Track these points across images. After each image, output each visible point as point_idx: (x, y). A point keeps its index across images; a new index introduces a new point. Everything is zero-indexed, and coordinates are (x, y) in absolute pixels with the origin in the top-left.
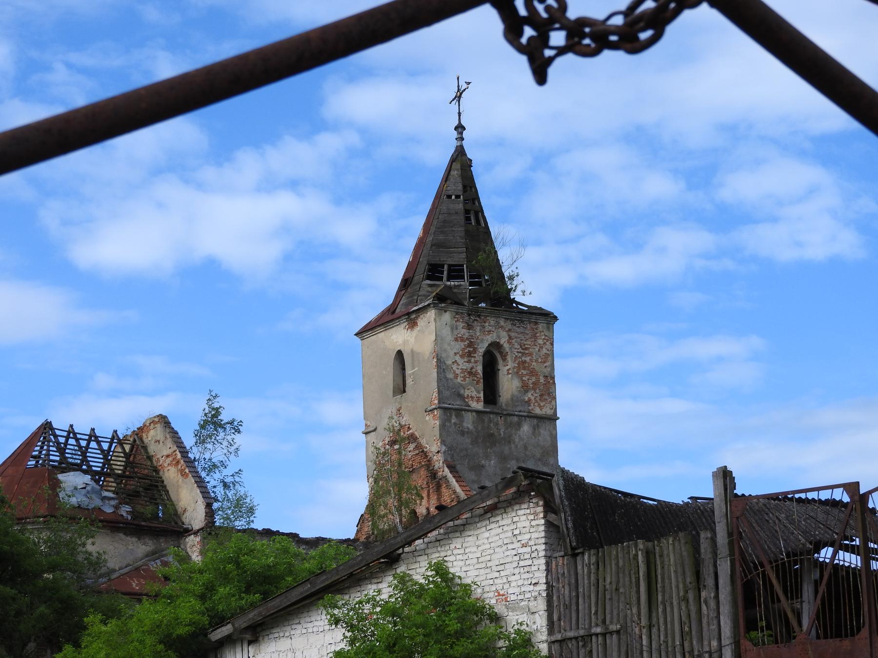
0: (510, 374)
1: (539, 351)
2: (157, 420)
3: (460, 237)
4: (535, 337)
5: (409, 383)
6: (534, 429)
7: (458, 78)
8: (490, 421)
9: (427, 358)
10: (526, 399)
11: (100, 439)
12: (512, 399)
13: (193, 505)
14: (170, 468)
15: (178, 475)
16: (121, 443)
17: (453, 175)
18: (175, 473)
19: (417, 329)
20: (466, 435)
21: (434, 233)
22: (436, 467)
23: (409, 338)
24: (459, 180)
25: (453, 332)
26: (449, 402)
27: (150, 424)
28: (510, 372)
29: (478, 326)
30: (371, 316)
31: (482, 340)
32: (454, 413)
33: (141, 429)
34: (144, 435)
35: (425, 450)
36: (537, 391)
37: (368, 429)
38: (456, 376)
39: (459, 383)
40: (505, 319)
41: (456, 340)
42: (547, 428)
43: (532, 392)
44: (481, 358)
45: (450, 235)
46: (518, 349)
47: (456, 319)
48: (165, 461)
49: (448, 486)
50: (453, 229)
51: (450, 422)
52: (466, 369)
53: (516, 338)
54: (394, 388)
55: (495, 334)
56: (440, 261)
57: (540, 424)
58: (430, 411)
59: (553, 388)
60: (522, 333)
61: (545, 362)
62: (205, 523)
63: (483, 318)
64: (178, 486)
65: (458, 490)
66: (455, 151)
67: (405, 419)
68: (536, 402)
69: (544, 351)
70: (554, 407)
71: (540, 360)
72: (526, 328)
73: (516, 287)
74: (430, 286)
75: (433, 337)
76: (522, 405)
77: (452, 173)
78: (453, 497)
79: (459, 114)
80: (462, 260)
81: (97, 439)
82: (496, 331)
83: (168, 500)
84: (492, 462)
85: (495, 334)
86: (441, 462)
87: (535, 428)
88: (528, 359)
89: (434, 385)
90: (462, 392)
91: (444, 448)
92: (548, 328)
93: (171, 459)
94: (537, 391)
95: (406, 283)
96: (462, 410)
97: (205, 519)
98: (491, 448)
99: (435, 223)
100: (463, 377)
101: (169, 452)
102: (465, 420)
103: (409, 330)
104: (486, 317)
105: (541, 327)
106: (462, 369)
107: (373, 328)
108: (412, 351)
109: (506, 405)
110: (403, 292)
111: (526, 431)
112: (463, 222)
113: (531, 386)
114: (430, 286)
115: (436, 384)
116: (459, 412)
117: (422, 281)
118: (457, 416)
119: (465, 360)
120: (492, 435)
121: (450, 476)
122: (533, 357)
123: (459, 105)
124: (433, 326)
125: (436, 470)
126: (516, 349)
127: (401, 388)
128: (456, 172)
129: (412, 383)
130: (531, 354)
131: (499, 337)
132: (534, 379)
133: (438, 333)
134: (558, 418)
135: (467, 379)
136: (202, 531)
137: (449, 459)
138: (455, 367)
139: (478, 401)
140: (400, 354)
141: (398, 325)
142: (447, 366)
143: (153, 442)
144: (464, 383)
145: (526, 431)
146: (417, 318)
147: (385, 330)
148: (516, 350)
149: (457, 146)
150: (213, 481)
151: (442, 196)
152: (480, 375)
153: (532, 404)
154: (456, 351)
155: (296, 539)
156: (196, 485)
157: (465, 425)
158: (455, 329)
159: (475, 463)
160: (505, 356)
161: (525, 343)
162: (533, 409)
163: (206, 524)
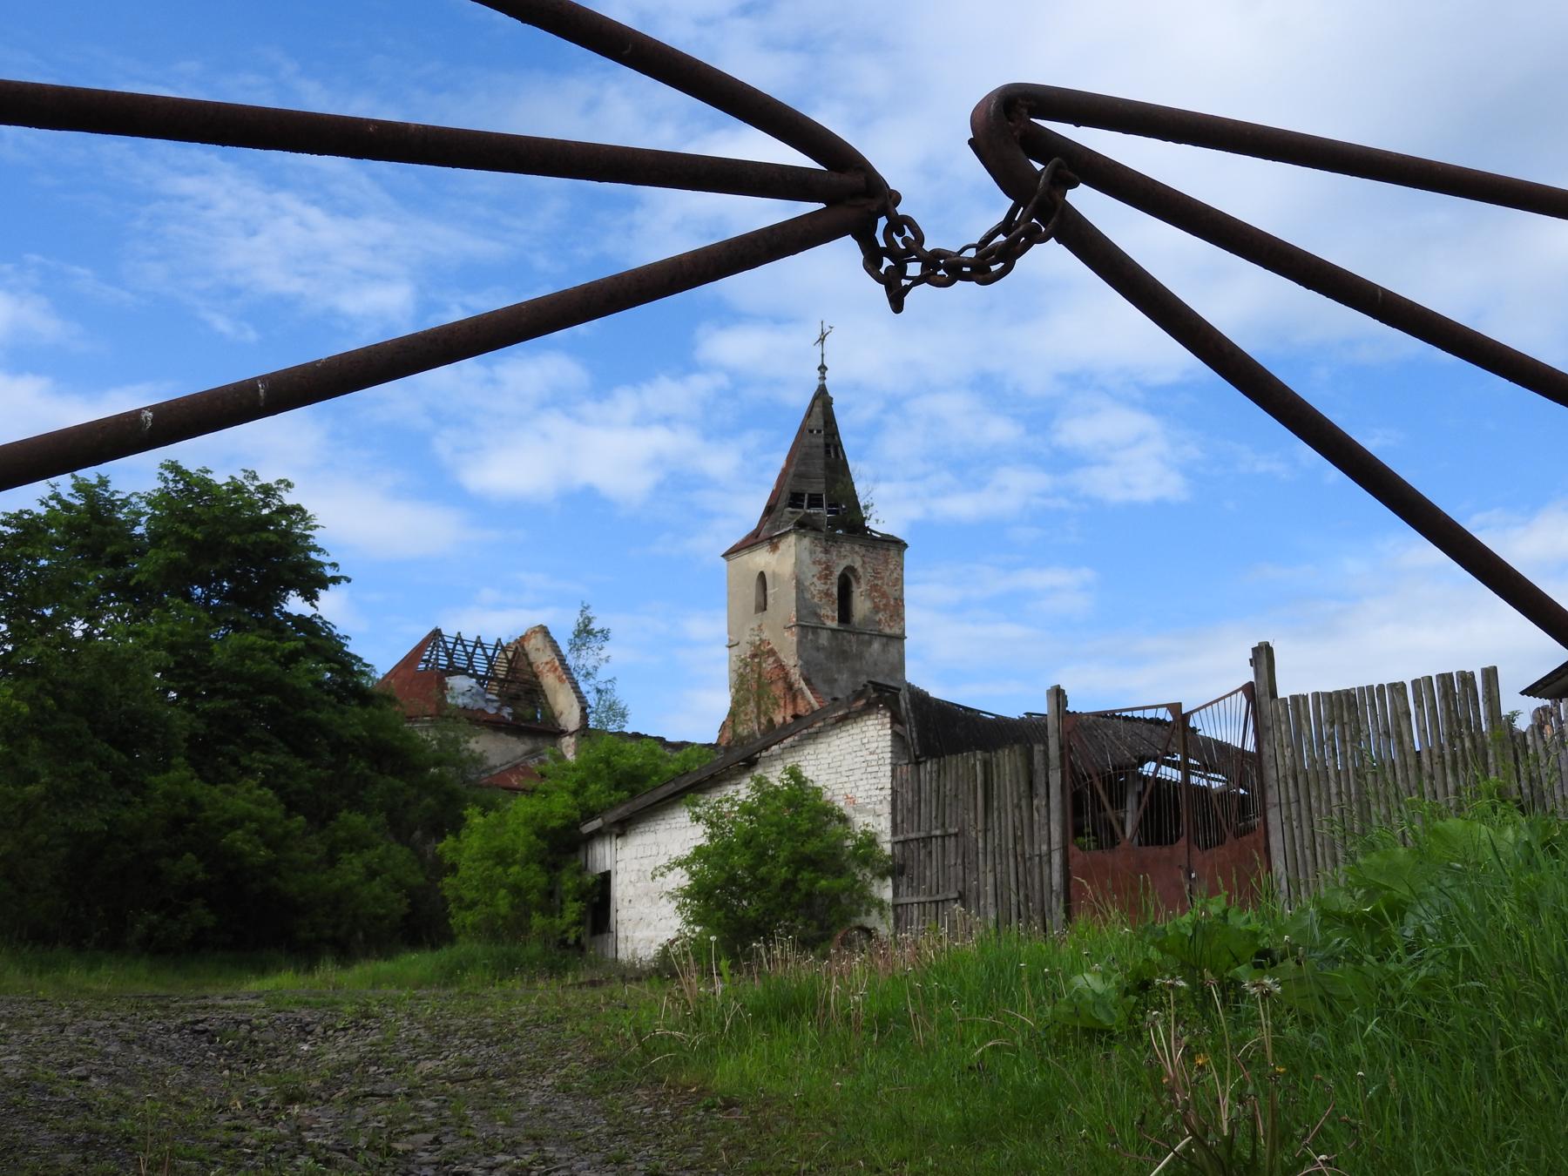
4: (886, 562)
16: (504, 650)
22: (793, 680)
24: (821, 416)
31: (838, 564)
34: (526, 644)
41: (814, 563)
49: (804, 697)
69: (895, 575)
75: (793, 560)
87: (885, 646)
88: (879, 582)
89: (794, 604)
90: (818, 611)
91: (800, 662)
92: (899, 554)
95: (769, 510)
96: (817, 628)
99: (797, 455)
101: (548, 659)
105: (892, 553)
114: (792, 513)
116: (815, 629)
118: (813, 633)
120: (844, 652)
124: (793, 550)
127: (762, 606)
131: (853, 561)
132: (884, 601)
138: (812, 588)
139: (833, 619)
140: (762, 575)
146: (779, 542)
157: (821, 641)
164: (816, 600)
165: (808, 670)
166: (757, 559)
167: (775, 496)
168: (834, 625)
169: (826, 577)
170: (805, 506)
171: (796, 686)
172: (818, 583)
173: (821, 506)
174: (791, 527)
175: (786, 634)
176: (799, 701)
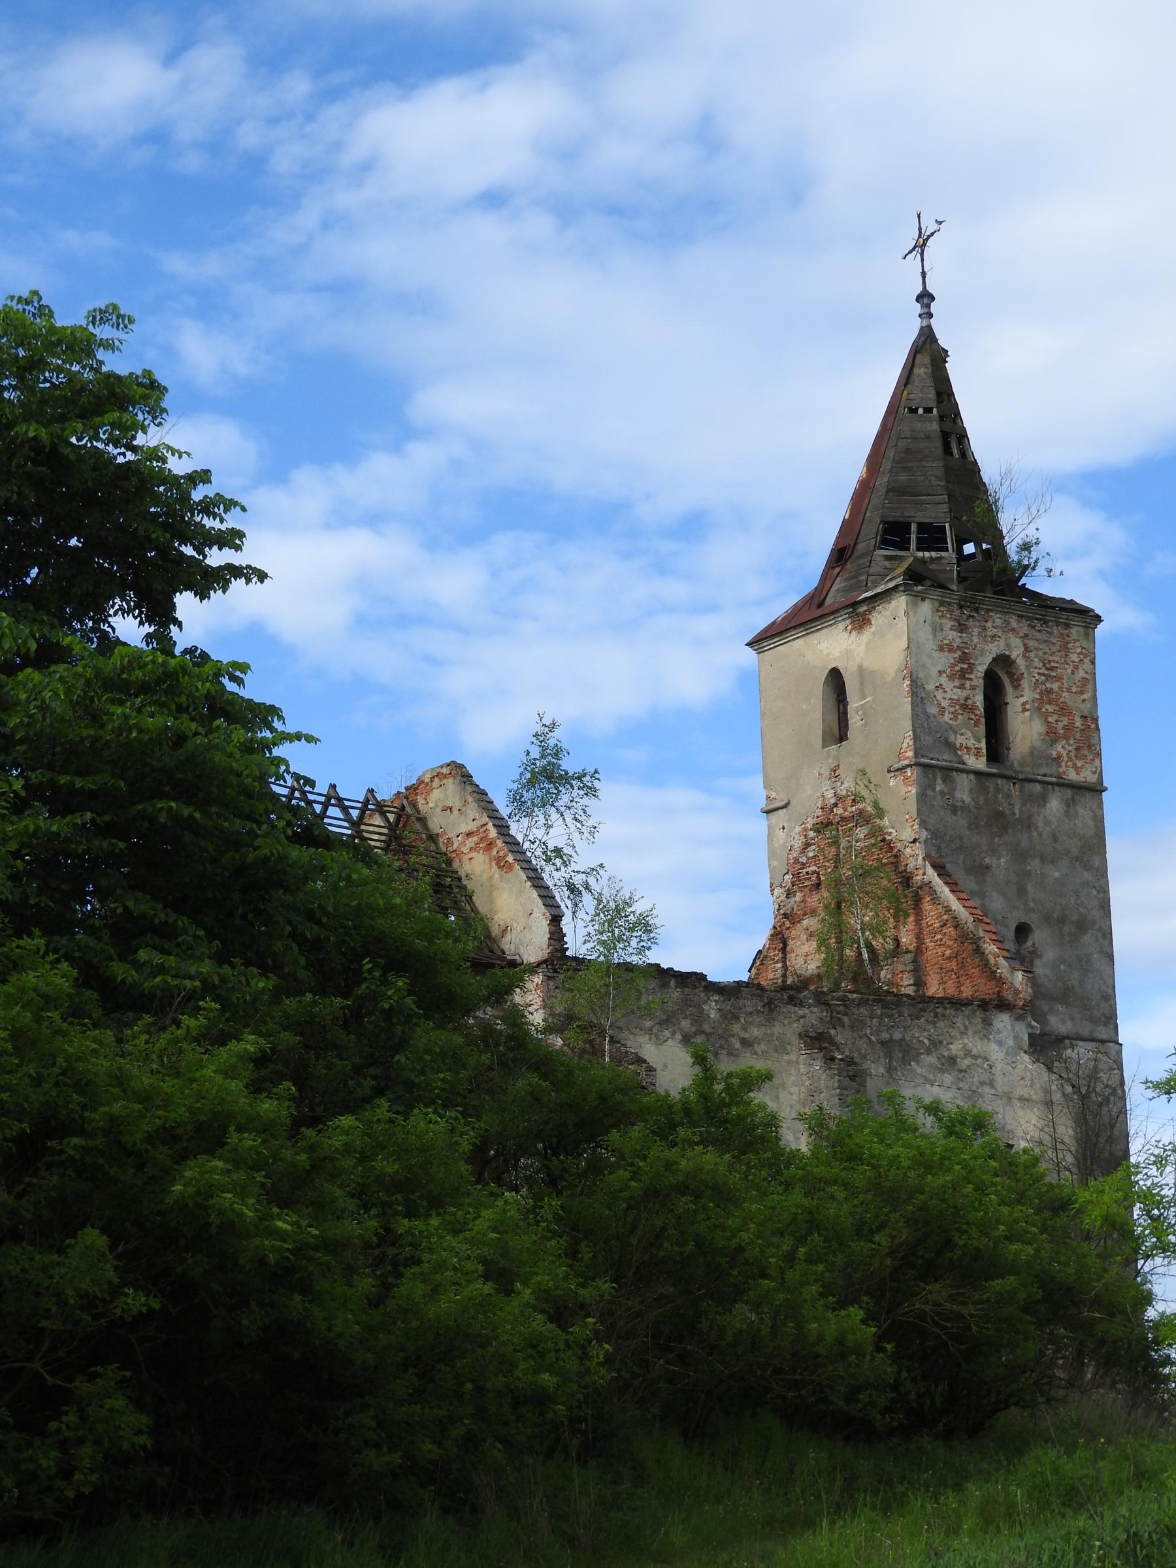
0: (1028, 710)
1: (1073, 673)
2: (445, 771)
3: (937, 477)
4: (1065, 649)
5: (855, 723)
6: (1068, 806)
7: (919, 216)
8: (998, 790)
9: (890, 678)
10: (1054, 754)
11: (347, 803)
12: (1031, 753)
13: (522, 920)
14: (474, 854)
15: (490, 868)
16: (381, 808)
17: (919, 375)
18: (484, 862)
19: (868, 632)
20: (959, 813)
21: (890, 471)
22: (911, 867)
23: (854, 646)
24: (929, 382)
25: (935, 635)
26: (932, 755)
27: (432, 779)
28: (1028, 707)
29: (975, 626)
30: (779, 609)
31: (983, 651)
32: (939, 775)
33: (412, 789)
34: (420, 800)
35: (888, 838)
36: (1071, 742)
37: (772, 804)
38: (942, 711)
39: (947, 723)
40: (1019, 616)
41: (941, 649)
42: (1088, 806)
43: (1064, 743)
44: (981, 681)
45: (919, 473)
46: (1040, 668)
47: (940, 614)
48: (463, 843)
49: (935, 899)
50: (923, 463)
51: (934, 789)
52: (958, 700)
53: (1036, 649)
54: (824, 732)
55: (1002, 642)
56: (903, 517)
57: (1077, 798)
58: (899, 769)
59: (1097, 738)
60: (1045, 641)
61: (1082, 693)
62: (548, 951)
63: (983, 613)
64: (492, 886)
65: (955, 905)
66: (920, 335)
67: (846, 785)
68: (1070, 759)
69: (1081, 673)
70: (1099, 769)
71: (1074, 689)
72: (1051, 633)
73: (1036, 562)
74: (889, 558)
76: (1047, 764)
77: (916, 371)
78: (945, 917)
79: (924, 274)
80: (942, 515)
81: (341, 803)
82: (1004, 637)
83: (473, 911)
84: (1003, 860)
85: (1002, 642)
86: (920, 858)
87: (1069, 804)
88: (1055, 686)
89: (908, 725)
90: (952, 738)
92: (1087, 635)
93: (475, 839)
94: (1071, 742)
95: (840, 555)
96: (952, 769)
97: (550, 945)
98: (1000, 837)
99: (891, 453)
100: (952, 713)
101: (472, 826)
102: (958, 788)
103: (854, 633)
105: (1075, 632)
106: (951, 699)
107: (782, 632)
108: (861, 669)
109: (1020, 764)
110: (837, 570)
111: (1054, 810)
112: (940, 451)
113: (1062, 732)
114: (889, 558)
115: (910, 723)
116: (948, 772)
117: (874, 550)
118: (944, 780)
119: (956, 684)
120: (1000, 815)
121: (937, 882)
122: (1063, 684)
123: (922, 260)
124: (902, 624)
125: (910, 873)
126: (1036, 668)
127: (839, 732)
128: (922, 370)
129: (860, 723)
130: (1059, 678)
131: (1008, 646)
133: (912, 636)
134: (1106, 789)
135: (960, 717)
136: (545, 966)
137: (933, 854)
138: (939, 695)
139: (978, 754)
140: (836, 678)
141: (831, 625)
142: (928, 693)
143: (438, 810)
144: (955, 723)
145: (1054, 810)
146: (869, 611)
147: (808, 634)
148: (1037, 671)
149: (922, 327)
150: (553, 877)
151: (900, 409)
152: (979, 710)
153: (1063, 764)
154: (942, 669)
155: (703, 983)
156: (529, 884)
157: (958, 795)
158: (938, 630)
159: (974, 861)
160: (1018, 680)
161: (1050, 658)
162: (1064, 772)
163: (551, 953)
164: (947, 717)
165: (939, 849)
166: (823, 646)
167: (849, 530)
168: (980, 764)
169: (963, 675)
170: (913, 545)
171: (918, 878)
172: (948, 685)
173: (946, 549)
174: (899, 580)
175: (892, 783)
176: (926, 906)
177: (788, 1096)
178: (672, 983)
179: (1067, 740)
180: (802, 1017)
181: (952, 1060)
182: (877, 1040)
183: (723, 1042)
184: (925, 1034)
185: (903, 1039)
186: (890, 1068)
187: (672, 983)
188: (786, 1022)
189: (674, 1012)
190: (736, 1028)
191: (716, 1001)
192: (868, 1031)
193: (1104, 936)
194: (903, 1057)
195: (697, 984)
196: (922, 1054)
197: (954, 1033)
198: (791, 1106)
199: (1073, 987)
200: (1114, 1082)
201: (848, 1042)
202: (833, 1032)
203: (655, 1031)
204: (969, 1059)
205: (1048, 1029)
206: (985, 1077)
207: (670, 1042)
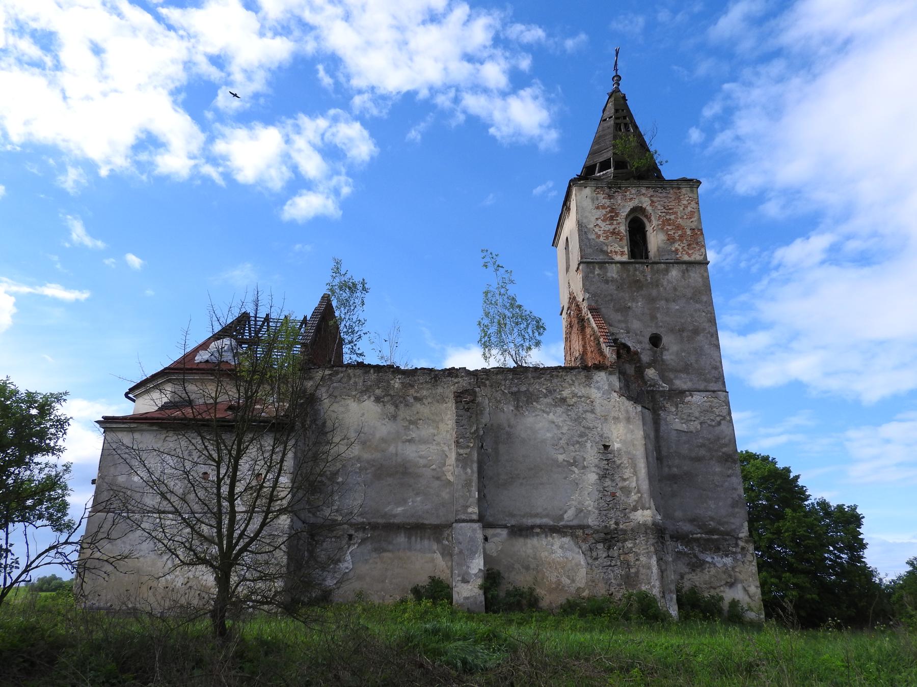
1: (684, 209)
4: (679, 199)
6: (684, 273)
8: (636, 270)
20: (610, 283)
36: (685, 242)
38: (599, 237)
40: (647, 187)
53: (659, 201)
59: (702, 239)
61: (691, 218)
70: (704, 253)
71: (685, 217)
88: (672, 217)
90: (605, 248)
94: (685, 242)
102: (609, 271)
104: (626, 188)
116: (602, 264)
118: (600, 268)
119: (608, 223)
131: (640, 202)
139: (622, 253)
142: (589, 229)
159: (621, 305)
160: (650, 218)
177: (445, 426)
178: (372, 371)
179: (682, 241)
180: (456, 383)
181: (563, 400)
182: (509, 392)
183: (402, 399)
184: (544, 387)
185: (528, 390)
186: (517, 407)
187: (372, 371)
188: (445, 386)
189: (371, 386)
190: (412, 391)
191: (399, 378)
192: (503, 388)
193: (712, 336)
194: (527, 400)
195: (387, 370)
196: (541, 397)
197: (566, 385)
198: (447, 431)
199: (691, 364)
200: (724, 413)
201: (488, 395)
202: (477, 389)
203: (357, 396)
204: (576, 399)
205: (674, 387)
206: (588, 408)
207: (367, 402)
